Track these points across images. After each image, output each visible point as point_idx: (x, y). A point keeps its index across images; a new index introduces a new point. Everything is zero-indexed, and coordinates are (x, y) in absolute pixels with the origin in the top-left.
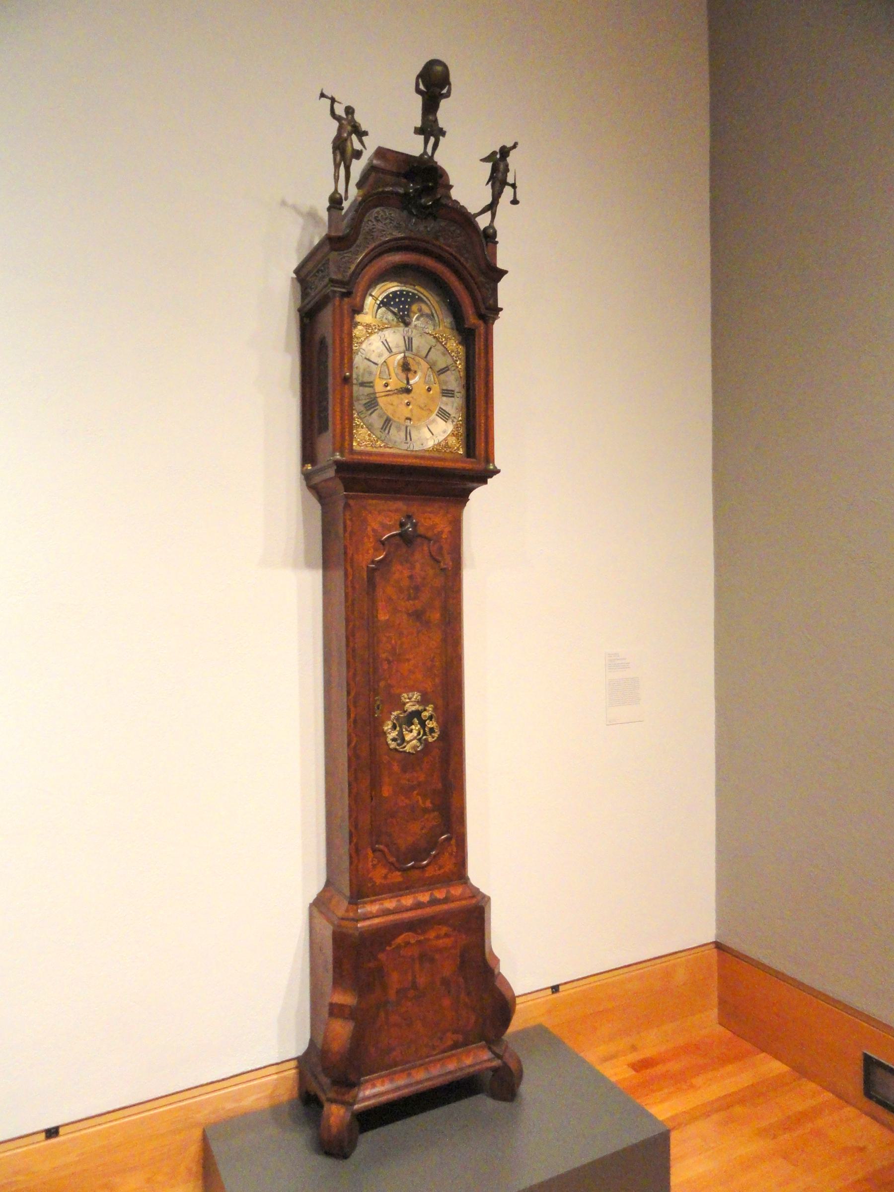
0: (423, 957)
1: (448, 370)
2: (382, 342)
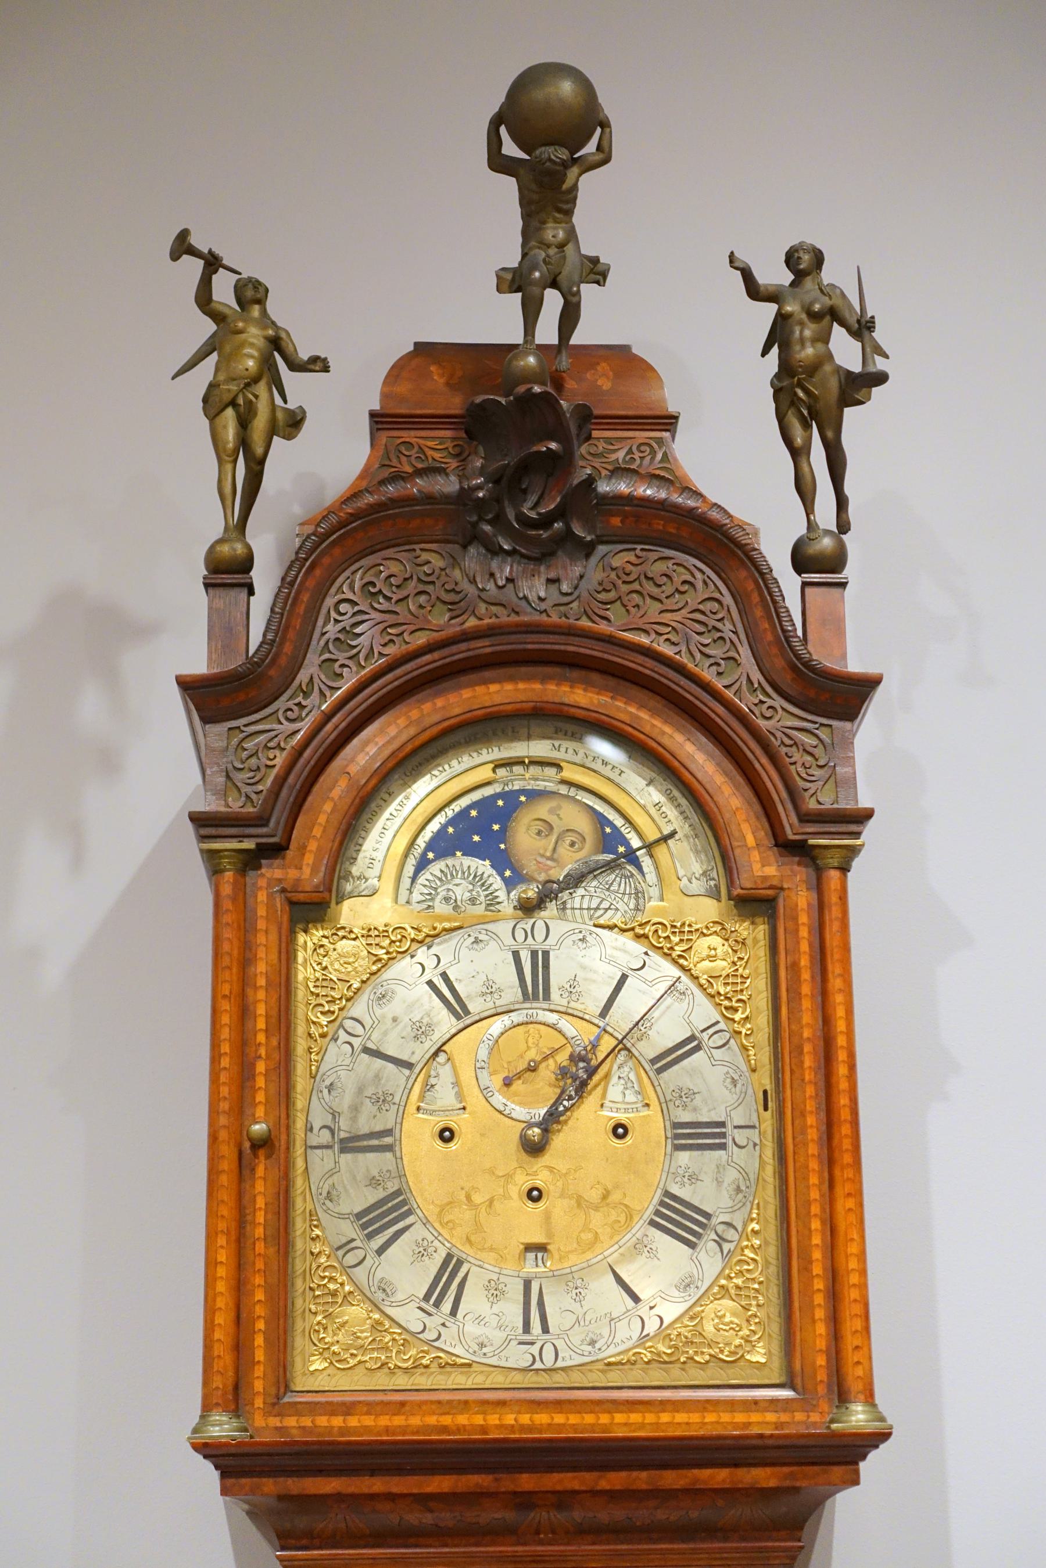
1: (698, 1048)
2: (430, 983)
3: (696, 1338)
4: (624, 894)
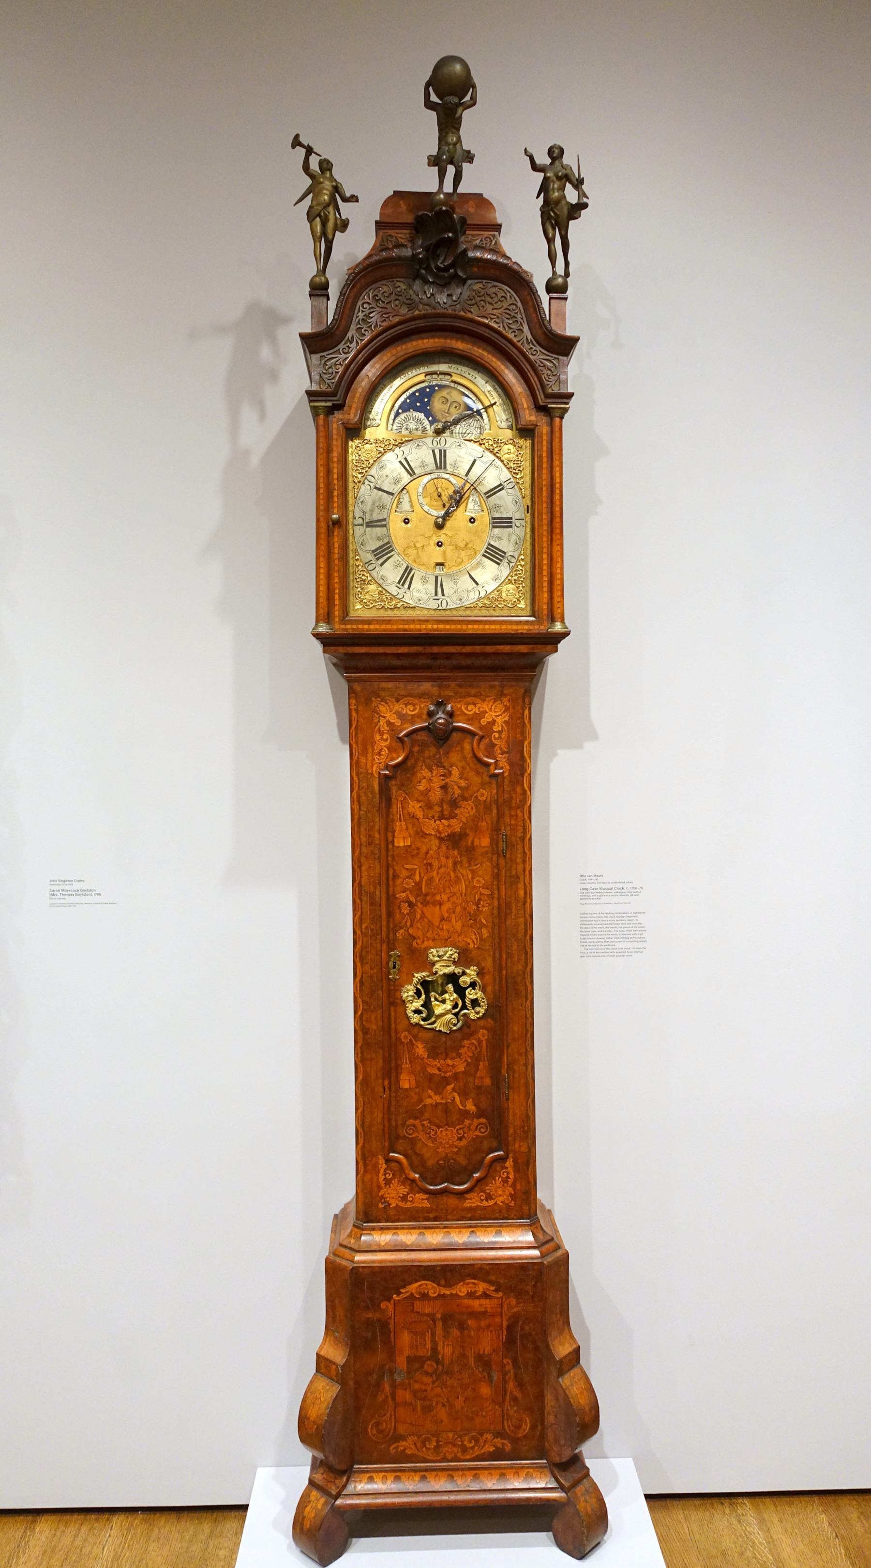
0: (447, 1319)
1: (503, 489)
2: (400, 462)
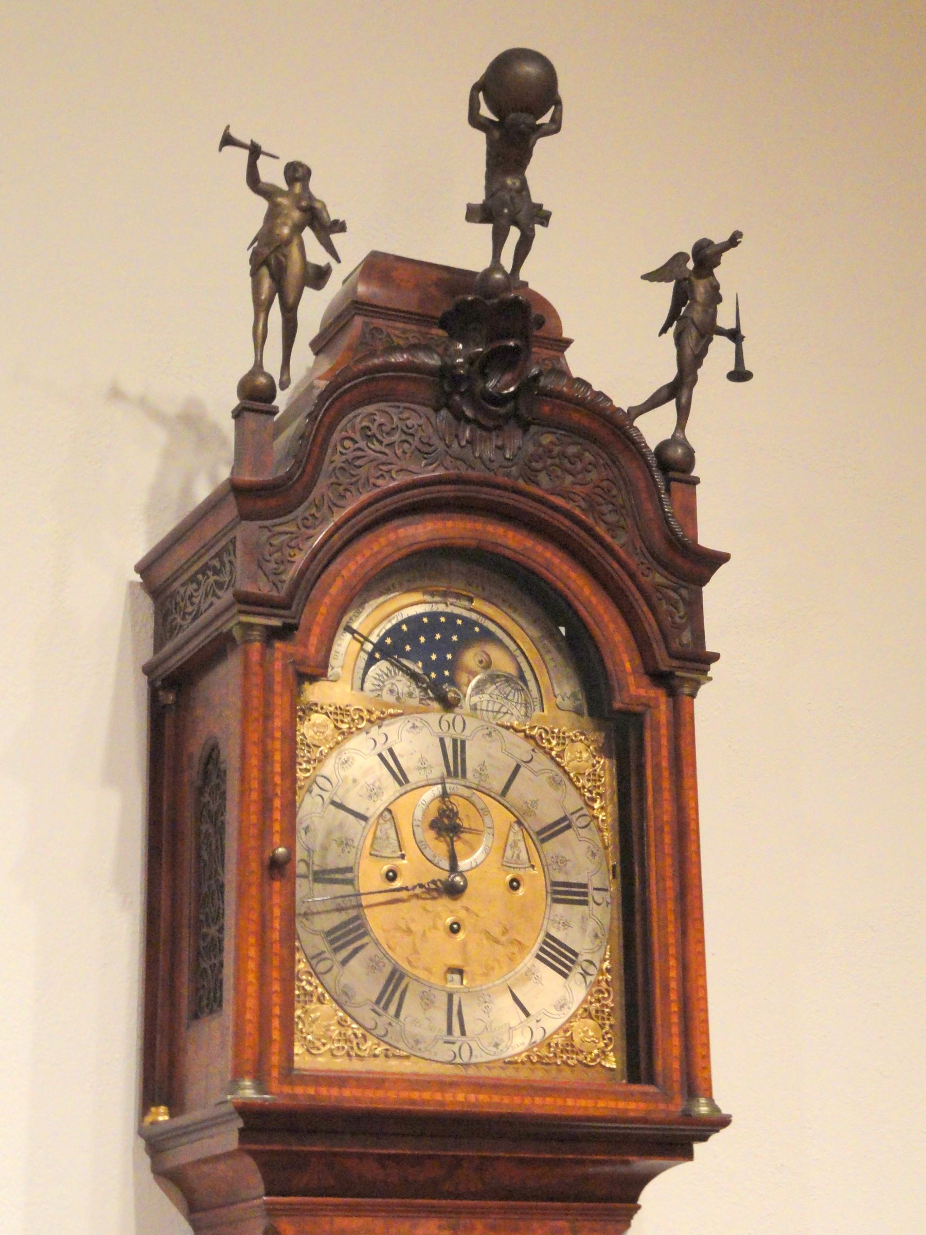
1: (569, 827)
2: (381, 756)
3: (569, 1047)
4: (517, 703)
